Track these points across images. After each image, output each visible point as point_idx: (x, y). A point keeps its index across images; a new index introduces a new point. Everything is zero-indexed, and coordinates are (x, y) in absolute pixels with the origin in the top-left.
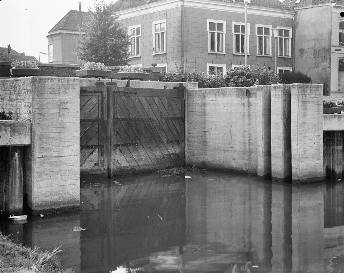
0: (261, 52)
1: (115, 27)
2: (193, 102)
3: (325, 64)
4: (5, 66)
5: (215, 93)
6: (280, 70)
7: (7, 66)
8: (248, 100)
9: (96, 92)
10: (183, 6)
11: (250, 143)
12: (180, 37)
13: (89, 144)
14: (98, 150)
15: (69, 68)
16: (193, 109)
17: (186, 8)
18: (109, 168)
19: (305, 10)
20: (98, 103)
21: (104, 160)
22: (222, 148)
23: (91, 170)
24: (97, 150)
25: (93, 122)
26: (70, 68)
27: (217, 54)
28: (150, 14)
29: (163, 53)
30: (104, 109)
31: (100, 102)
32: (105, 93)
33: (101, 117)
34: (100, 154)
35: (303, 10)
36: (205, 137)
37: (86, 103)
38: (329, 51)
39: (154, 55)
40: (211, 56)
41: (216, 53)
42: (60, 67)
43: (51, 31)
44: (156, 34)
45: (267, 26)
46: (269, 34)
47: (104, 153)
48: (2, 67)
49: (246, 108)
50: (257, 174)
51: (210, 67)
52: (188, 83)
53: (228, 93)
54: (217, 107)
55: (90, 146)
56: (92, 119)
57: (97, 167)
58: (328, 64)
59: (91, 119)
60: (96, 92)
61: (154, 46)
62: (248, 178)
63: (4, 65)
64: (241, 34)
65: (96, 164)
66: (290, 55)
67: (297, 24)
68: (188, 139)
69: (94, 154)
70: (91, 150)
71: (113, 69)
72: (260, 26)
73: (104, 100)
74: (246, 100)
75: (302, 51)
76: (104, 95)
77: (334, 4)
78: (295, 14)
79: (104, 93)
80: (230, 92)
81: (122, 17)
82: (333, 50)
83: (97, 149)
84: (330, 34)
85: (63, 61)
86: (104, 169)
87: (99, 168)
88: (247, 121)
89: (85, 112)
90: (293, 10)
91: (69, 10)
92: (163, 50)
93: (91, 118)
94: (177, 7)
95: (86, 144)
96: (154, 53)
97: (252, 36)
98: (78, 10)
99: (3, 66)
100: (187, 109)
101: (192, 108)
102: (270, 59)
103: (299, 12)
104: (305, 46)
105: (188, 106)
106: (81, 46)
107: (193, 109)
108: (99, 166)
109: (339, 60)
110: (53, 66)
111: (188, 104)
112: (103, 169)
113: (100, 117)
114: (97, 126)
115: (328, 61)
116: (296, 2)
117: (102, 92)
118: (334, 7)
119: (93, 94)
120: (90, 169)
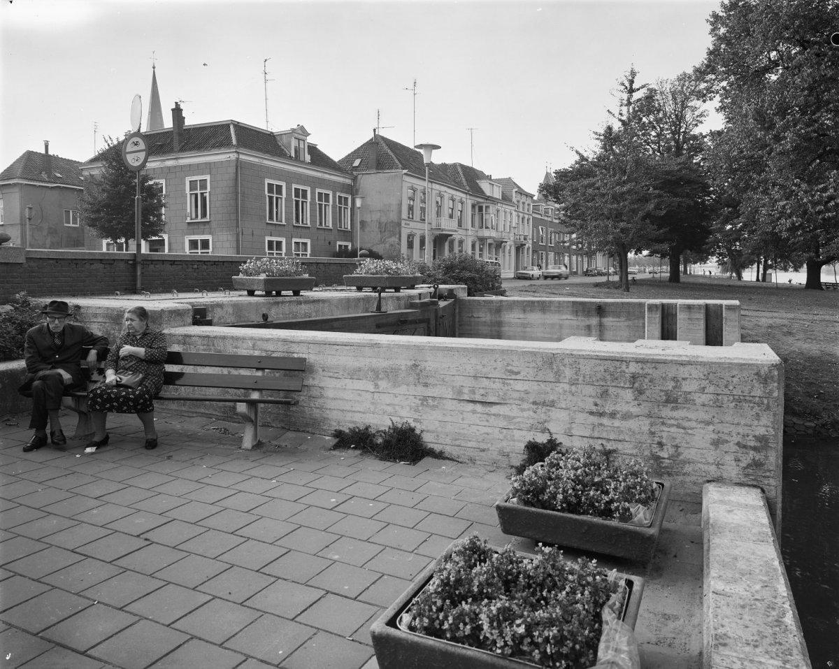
0: (321, 224)
2: (472, 319)
3: (394, 240)
6: (340, 246)
8: (600, 321)
9: (421, 321)
10: (238, 159)
16: (471, 330)
17: (241, 162)
18: (427, 461)
19: (367, 176)
27: (276, 224)
28: (182, 167)
32: (433, 322)
35: (364, 176)
38: (399, 225)
40: (270, 227)
41: (199, 221)
44: (191, 194)
45: (327, 192)
48: (171, 264)
53: (552, 308)
54: (528, 329)
58: (397, 240)
61: (189, 210)
64: (301, 200)
66: (349, 228)
67: (357, 191)
74: (594, 321)
75: (363, 223)
76: (432, 327)
77: (405, 171)
78: (355, 179)
80: (559, 307)
82: (403, 223)
84: (400, 205)
85: (469, 295)
91: (25, 151)
92: (204, 215)
94: (229, 159)
96: (189, 220)
98: (43, 152)
99: (172, 263)
101: (469, 328)
102: (308, 231)
103: (359, 177)
104: (368, 218)
105: (460, 325)
106: (86, 206)
107: (471, 330)
115: (398, 236)
116: (354, 165)
118: (405, 174)
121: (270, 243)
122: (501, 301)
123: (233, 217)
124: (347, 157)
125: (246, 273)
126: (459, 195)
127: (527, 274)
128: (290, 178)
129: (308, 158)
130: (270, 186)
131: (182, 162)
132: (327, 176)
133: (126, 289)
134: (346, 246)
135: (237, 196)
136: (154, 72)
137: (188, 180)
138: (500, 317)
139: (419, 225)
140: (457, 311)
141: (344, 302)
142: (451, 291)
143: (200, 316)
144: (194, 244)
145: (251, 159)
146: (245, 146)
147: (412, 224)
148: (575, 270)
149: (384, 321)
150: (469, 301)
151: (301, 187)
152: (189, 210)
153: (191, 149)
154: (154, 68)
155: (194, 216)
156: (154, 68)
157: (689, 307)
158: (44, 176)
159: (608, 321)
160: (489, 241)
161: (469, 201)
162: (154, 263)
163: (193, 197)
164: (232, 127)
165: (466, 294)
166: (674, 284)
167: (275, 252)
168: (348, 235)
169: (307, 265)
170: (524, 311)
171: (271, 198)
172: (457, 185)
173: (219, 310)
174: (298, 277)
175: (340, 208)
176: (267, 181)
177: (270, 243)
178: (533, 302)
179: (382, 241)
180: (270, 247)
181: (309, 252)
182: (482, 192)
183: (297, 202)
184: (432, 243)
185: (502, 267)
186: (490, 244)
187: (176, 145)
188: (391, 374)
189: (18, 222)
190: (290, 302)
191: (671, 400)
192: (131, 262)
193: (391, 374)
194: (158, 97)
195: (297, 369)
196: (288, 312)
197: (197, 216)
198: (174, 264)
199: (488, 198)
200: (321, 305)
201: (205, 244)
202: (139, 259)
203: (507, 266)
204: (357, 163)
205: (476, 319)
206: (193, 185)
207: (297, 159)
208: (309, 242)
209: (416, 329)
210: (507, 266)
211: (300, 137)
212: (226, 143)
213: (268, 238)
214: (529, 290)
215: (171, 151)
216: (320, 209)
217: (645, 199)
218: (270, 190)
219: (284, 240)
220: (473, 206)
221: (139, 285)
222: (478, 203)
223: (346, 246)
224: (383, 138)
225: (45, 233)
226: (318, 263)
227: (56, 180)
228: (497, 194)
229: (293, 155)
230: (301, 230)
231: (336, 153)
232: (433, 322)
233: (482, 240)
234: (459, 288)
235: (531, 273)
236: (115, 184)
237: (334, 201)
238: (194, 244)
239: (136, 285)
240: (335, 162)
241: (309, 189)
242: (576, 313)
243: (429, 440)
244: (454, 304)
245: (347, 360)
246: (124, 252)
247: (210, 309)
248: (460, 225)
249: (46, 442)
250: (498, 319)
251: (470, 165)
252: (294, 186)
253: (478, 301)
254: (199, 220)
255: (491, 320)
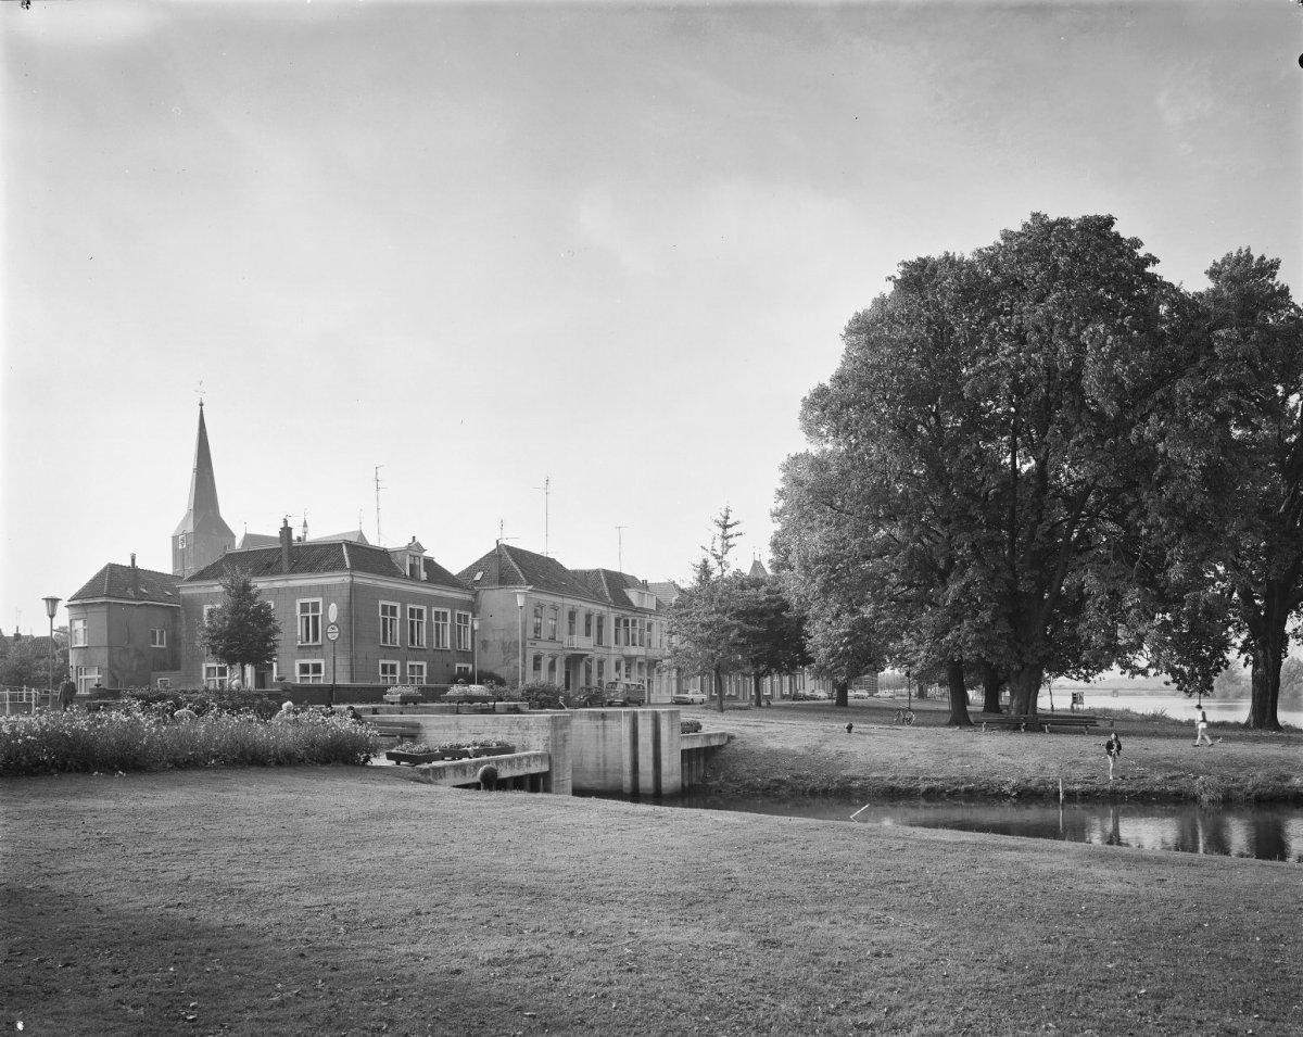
0: (438, 644)
1: (260, 607)
6: (460, 668)
11: (605, 765)
12: (1049, 707)
19: (490, 592)
28: (292, 589)
29: (316, 644)
39: (300, 647)
43: (72, 599)
45: (393, 604)
46: (395, 615)
49: (601, 731)
50: (622, 791)
51: (383, 665)
61: (299, 634)
62: (1040, 807)
67: (479, 607)
72: (385, 603)
74: (600, 723)
75: (485, 644)
78: (476, 595)
81: (260, 586)
85: (352, 679)
88: (601, 744)
90: (473, 589)
92: (316, 638)
96: (299, 643)
97: (403, 620)
98: (128, 563)
103: (481, 593)
109: (582, 656)
121: (384, 666)
123: (347, 640)
124: (467, 570)
125: (391, 693)
126: (597, 609)
128: (404, 597)
129: (424, 575)
130: (384, 607)
131: (292, 583)
132: (444, 594)
134: (466, 669)
135: (351, 620)
136: (201, 411)
137: (298, 602)
139: (550, 645)
143: (375, 711)
144: (304, 669)
145: (365, 581)
146: (359, 569)
147: (539, 644)
148: (769, 693)
151: (417, 607)
152: (299, 634)
153: (302, 571)
154: (201, 405)
155: (304, 640)
156: (201, 405)
157: (644, 712)
158: (130, 592)
159: (608, 722)
160: (639, 660)
161: (611, 616)
163: (304, 620)
164: (344, 547)
166: (842, 709)
168: (468, 656)
169: (421, 689)
171: (385, 620)
172: (598, 598)
175: (459, 627)
176: (381, 603)
177: (384, 666)
179: (506, 663)
180: (384, 671)
181: (425, 675)
182: (630, 603)
183: (412, 623)
184: (564, 665)
186: (640, 664)
187: (285, 564)
188: (449, 727)
189: (106, 643)
191: (527, 729)
193: (449, 727)
194: (206, 436)
195: (418, 726)
197: (308, 639)
199: (637, 610)
201: (317, 668)
204: (478, 577)
206: (304, 607)
207: (414, 576)
208: (425, 664)
211: (415, 554)
212: (337, 566)
213: (381, 662)
215: (279, 572)
216: (438, 631)
217: (727, 629)
218: (384, 612)
219: (398, 664)
220: (617, 621)
222: (623, 616)
223: (466, 669)
224: (508, 548)
225: (132, 654)
227: (141, 596)
228: (650, 604)
229: (408, 573)
230: (418, 653)
231: (455, 565)
233: (630, 660)
235: (819, 695)
236: (234, 612)
237: (452, 620)
238: (304, 669)
240: (452, 575)
241: (425, 608)
242: (590, 718)
243: (282, 525)
245: (434, 723)
248: (600, 642)
251: (617, 570)
252: (409, 606)
254: (311, 643)
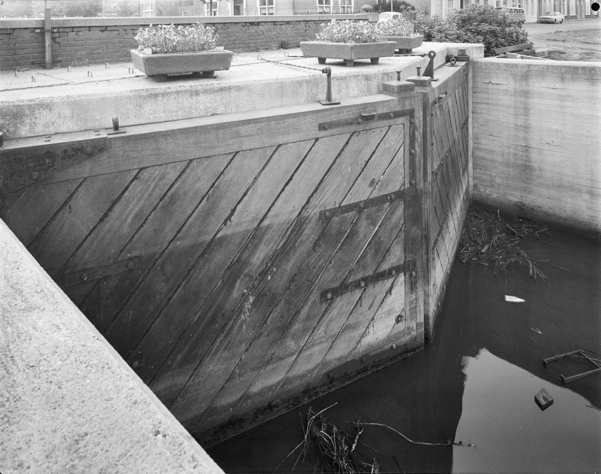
4: (108, 29)
5: (562, 74)
7: (114, 28)
9: (397, 115)
13: (385, 267)
14: (403, 277)
15: (244, 24)
16: (488, 99)
20: (403, 146)
21: (416, 299)
22: (584, 189)
23: (389, 339)
24: (402, 278)
25: (392, 201)
26: (246, 23)
30: (417, 159)
31: (407, 141)
32: (419, 114)
33: (411, 184)
34: (408, 286)
36: (528, 157)
37: (375, 151)
42: (228, 23)
47: (416, 283)
52: (474, 49)
54: (568, 104)
55: (384, 271)
56: (390, 195)
57: (401, 326)
59: (386, 196)
60: (397, 115)
63: (107, 27)
65: (399, 319)
68: (473, 153)
69: (393, 291)
70: (388, 283)
71: (315, 21)
73: (417, 133)
76: (417, 122)
79: (416, 113)
83: (402, 274)
86: (418, 325)
87: (406, 326)
89: (372, 178)
93: (387, 193)
95: (376, 270)
99: (104, 28)
100: (473, 97)
101: (487, 96)
108: (406, 320)
110: (215, 22)
111: (473, 87)
112: (414, 325)
113: (407, 185)
114: (400, 211)
117: (411, 113)
119: (391, 122)
120: (386, 335)
122: (529, 66)
127: (549, 19)
133: (33, 63)
138: (527, 85)
140: (470, 75)
141: (274, 87)
142: (463, 52)
149: (334, 118)
150: (486, 64)
162: (75, 30)
165: (483, 54)
167: (324, 6)
170: (563, 79)
173: (45, 113)
174: (205, 53)
178: (576, 68)
185: (525, 13)
190: (177, 92)
192: (38, 31)
196: (175, 109)
198: (106, 30)
200: (234, 93)
202: (48, 27)
203: (530, 11)
205: (495, 87)
209: (390, 127)
210: (530, 11)
214: (558, 38)
221: (48, 57)
226: (307, 21)
232: (419, 114)
234: (473, 48)
235: (554, 17)
239: (44, 58)
244: (465, 70)
246: (340, 6)
247: (27, 112)
249: (378, 62)
250: (525, 88)
253: (497, 64)
255: (515, 89)
